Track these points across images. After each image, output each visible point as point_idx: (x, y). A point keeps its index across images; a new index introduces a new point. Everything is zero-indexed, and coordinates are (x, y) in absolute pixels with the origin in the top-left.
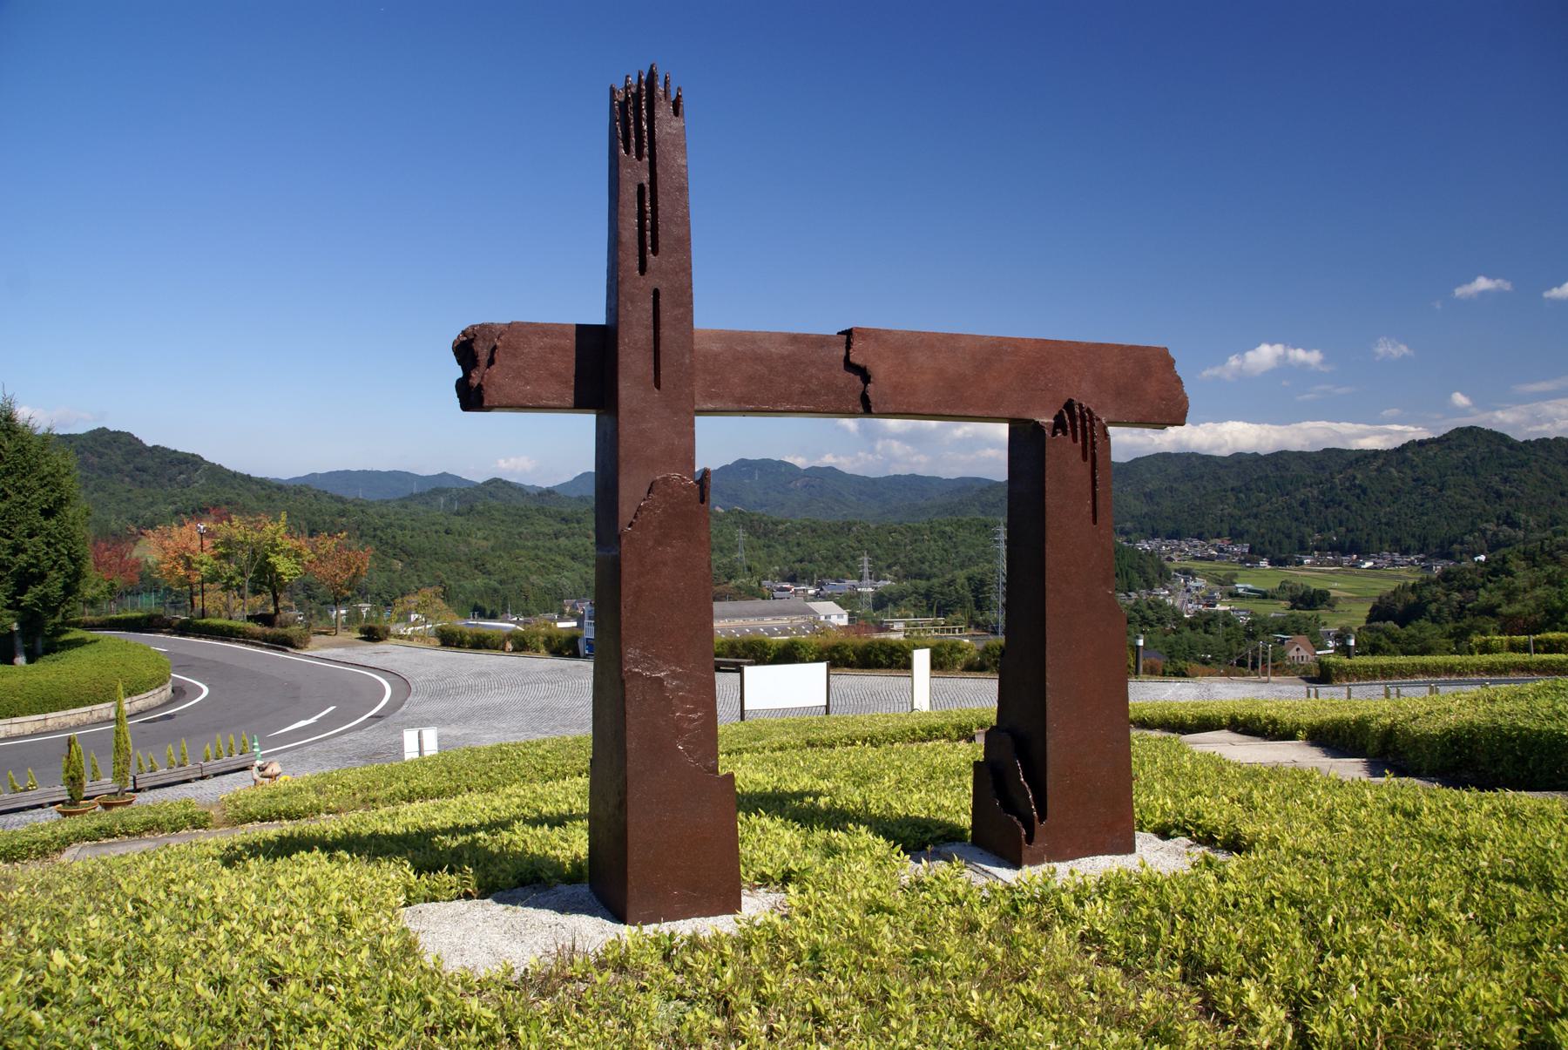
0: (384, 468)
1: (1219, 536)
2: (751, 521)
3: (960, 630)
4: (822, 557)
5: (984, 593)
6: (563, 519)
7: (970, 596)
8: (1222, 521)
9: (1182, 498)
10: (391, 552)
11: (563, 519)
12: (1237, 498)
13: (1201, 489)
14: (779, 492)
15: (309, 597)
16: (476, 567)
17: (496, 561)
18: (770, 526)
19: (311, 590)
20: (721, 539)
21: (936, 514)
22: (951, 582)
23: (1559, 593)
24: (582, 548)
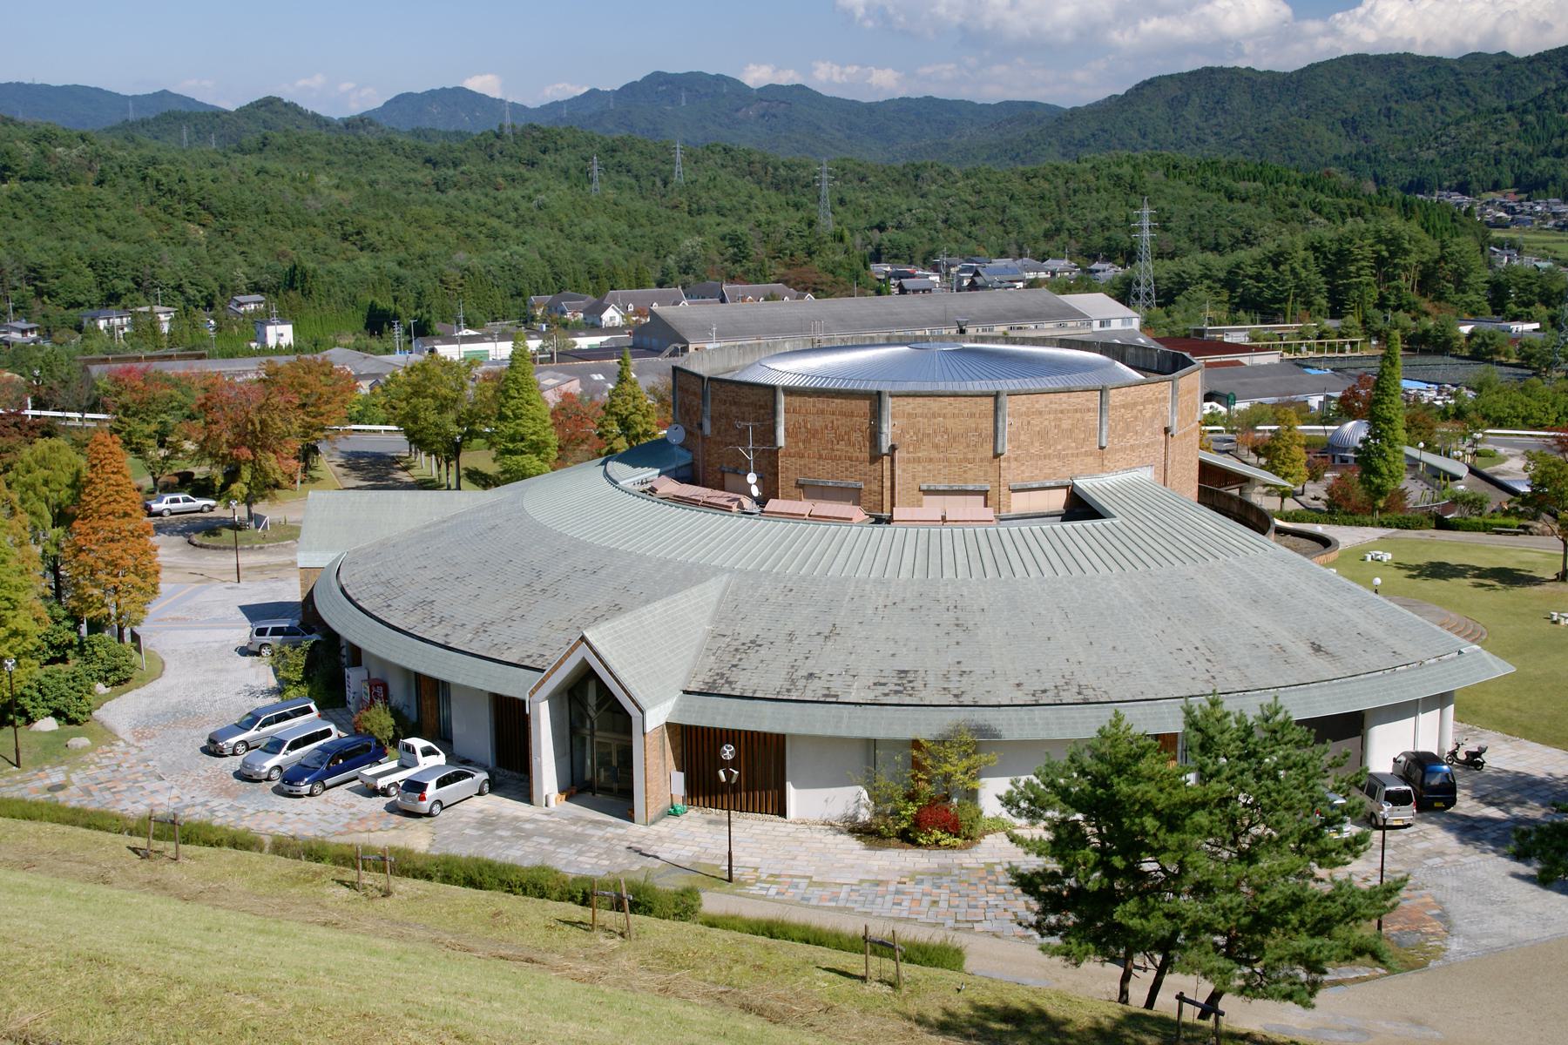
0: (56, 80)
1: (1496, 186)
2: (750, 163)
3: (1353, 344)
4: (918, 220)
5: (1347, 275)
6: (428, 161)
7: (1321, 281)
8: (1498, 162)
9: (1407, 128)
10: (181, 208)
11: (428, 161)
12: (1522, 123)
13: (1438, 112)
14: (720, 125)
15: (39, 293)
16: (345, 238)
17: (382, 225)
18: (782, 171)
19: (42, 279)
20: (715, 193)
21: (988, 159)
22: (1276, 260)
23: (546, 444)
24: (509, 206)
